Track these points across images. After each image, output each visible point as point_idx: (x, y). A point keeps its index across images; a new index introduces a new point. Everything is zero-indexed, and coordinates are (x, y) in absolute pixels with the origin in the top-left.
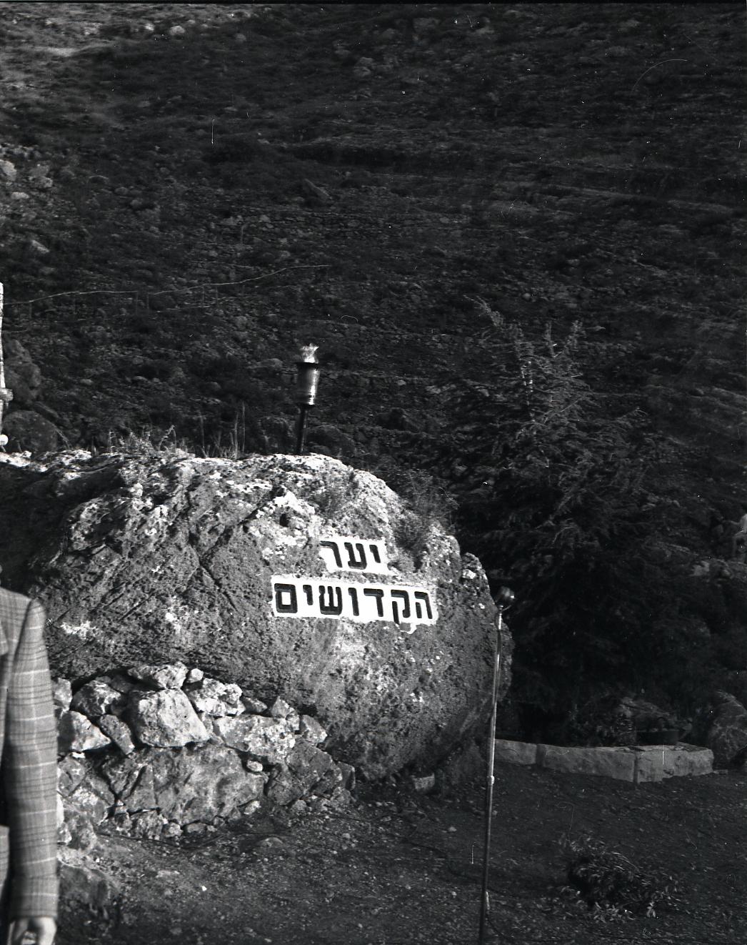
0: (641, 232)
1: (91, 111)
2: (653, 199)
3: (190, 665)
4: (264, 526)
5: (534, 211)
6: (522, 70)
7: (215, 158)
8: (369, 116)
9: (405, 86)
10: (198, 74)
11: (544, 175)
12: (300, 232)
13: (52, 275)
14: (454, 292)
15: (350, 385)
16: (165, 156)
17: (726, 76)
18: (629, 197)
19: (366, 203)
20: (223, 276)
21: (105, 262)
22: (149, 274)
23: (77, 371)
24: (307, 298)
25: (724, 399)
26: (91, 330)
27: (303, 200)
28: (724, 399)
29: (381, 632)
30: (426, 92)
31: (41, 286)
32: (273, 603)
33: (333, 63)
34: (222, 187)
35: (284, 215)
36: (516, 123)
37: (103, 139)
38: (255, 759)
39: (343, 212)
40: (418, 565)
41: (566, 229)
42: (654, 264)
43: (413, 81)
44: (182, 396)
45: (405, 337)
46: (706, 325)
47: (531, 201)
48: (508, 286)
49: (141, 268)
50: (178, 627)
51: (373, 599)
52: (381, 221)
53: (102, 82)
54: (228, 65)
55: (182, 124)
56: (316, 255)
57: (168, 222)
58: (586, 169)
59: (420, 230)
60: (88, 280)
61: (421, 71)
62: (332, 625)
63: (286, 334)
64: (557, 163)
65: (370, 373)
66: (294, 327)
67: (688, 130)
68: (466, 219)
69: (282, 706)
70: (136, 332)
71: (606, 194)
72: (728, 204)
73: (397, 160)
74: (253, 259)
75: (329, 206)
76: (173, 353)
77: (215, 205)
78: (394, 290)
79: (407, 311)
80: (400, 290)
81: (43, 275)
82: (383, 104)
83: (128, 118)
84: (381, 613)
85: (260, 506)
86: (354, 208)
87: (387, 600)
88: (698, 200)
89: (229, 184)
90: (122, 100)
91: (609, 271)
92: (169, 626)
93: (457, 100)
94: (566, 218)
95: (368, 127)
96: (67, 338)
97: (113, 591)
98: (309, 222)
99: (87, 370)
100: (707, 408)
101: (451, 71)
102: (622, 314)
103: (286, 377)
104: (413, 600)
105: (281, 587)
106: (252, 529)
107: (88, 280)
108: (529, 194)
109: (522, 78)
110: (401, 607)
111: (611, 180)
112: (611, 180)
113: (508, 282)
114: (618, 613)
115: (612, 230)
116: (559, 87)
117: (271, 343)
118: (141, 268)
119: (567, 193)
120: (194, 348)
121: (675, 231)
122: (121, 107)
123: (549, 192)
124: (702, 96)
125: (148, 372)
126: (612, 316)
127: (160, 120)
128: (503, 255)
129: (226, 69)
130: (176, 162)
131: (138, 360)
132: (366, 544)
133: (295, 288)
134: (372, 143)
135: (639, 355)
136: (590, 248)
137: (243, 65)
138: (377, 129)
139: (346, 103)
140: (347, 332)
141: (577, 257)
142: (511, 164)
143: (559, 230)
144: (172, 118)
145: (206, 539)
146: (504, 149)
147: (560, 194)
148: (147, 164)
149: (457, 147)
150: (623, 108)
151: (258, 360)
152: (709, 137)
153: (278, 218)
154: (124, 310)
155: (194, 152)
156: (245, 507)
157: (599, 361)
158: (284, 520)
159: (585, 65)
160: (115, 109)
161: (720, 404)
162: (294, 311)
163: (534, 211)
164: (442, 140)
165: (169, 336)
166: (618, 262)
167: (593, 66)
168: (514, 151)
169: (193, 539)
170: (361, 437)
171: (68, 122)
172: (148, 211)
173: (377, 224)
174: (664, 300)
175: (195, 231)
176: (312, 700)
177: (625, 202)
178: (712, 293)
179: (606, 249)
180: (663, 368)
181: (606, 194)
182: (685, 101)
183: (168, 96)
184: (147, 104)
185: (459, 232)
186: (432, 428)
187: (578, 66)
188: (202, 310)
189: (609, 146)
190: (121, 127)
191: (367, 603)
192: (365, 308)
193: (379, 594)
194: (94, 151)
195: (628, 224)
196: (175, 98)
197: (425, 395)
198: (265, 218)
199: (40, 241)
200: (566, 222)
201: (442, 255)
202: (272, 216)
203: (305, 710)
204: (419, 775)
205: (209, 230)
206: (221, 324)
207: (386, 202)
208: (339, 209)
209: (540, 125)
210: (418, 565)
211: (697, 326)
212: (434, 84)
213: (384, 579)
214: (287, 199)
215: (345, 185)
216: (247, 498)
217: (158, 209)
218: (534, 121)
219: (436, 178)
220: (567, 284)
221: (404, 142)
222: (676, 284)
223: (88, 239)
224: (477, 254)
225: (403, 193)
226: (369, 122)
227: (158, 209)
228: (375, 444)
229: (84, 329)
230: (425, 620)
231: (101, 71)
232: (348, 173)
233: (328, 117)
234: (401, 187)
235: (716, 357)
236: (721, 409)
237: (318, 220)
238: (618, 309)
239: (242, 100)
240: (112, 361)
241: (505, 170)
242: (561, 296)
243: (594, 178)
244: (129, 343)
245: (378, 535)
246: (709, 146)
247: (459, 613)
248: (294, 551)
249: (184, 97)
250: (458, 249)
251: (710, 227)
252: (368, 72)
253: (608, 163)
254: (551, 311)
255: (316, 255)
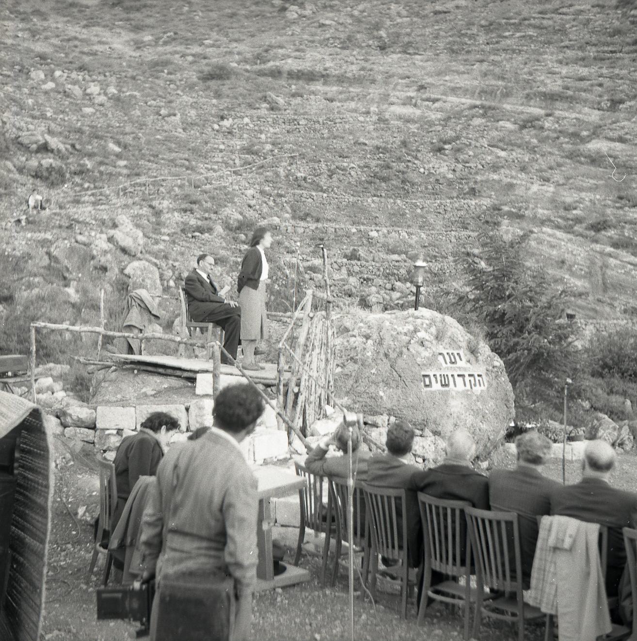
0: (487, 126)
1: (112, 43)
2: (493, 104)
3: (389, 415)
4: (414, 347)
5: (418, 112)
6: (399, 14)
7: (211, 77)
8: (301, 47)
9: (322, 25)
10: (182, 17)
11: (422, 88)
12: (271, 129)
13: (126, 166)
14: (377, 170)
15: (323, 233)
16: (172, 77)
17: (532, 21)
18: (478, 103)
19: (308, 107)
20: (231, 162)
21: (157, 156)
22: (187, 163)
23: (156, 231)
24: (287, 176)
25: (549, 235)
26: (160, 203)
27: (268, 106)
28: (549, 235)
29: (467, 395)
30: (337, 30)
31: (120, 174)
32: (422, 384)
33: (271, 10)
34: (215, 97)
35: (259, 118)
36: (400, 52)
37: (124, 64)
38: (419, 456)
39: (295, 114)
40: (477, 360)
41: (440, 124)
42: (498, 147)
43: (328, 22)
44: (224, 244)
45: (351, 200)
46: (535, 188)
47: (415, 105)
48: (410, 164)
49: (181, 159)
50: (385, 398)
51: (461, 379)
52: (321, 120)
53: (117, 23)
54: (202, 11)
55: (176, 52)
56: (287, 146)
57: (187, 126)
58: (449, 84)
59: (347, 126)
60: (149, 169)
61: (331, 15)
62: (447, 393)
63: (278, 200)
64: (429, 80)
65: (334, 225)
66: (281, 196)
67: (512, 58)
68: (375, 118)
69: (427, 432)
70: (189, 204)
71: (463, 100)
72: (541, 108)
73: (325, 77)
74: (249, 150)
75: (285, 110)
76: (213, 216)
77: (213, 112)
78: (340, 169)
79: (349, 183)
80: (344, 169)
81: (120, 167)
82: (311, 39)
83: (139, 48)
84: (465, 385)
85: (412, 338)
86: (302, 111)
87: (467, 379)
88: (522, 104)
89: (218, 95)
90: (132, 36)
91: (471, 153)
92: (381, 397)
93: (358, 36)
94: (439, 116)
95: (302, 54)
96: (145, 209)
97: (356, 382)
98: (275, 122)
99: (163, 230)
100: (540, 242)
101: (352, 16)
102: (482, 181)
103: (283, 228)
104: (477, 378)
105: (425, 376)
106: (411, 350)
107: (149, 169)
108: (414, 101)
109: (399, 20)
110: (473, 382)
111: (466, 92)
112: (466, 92)
113: (409, 161)
114: (25, 294)
115: (469, 125)
116: (424, 27)
117: (271, 208)
118: (181, 159)
119: (437, 100)
120: (226, 213)
121: (509, 126)
122: (133, 40)
123: (428, 100)
124: (518, 34)
125: (201, 230)
126: (476, 182)
127: (160, 49)
128: (404, 144)
129: (200, 14)
130: (181, 80)
131: (193, 222)
132: (455, 352)
133: (279, 169)
134: (304, 65)
135: (496, 208)
136: (458, 138)
137: (211, 11)
138: (308, 56)
139: (285, 38)
140: (315, 198)
141: (450, 143)
142: (400, 81)
143: (435, 125)
144: (169, 48)
145: (393, 355)
146: (394, 70)
147: (435, 101)
148: (161, 83)
149: (363, 69)
150: (469, 42)
151: (264, 218)
152: (526, 63)
153: (255, 119)
154: (176, 189)
155: (191, 73)
156: (406, 339)
157: (470, 212)
158: (422, 344)
159: (440, 12)
160: (127, 41)
161: (548, 239)
162: (280, 185)
163: (418, 112)
164: (352, 64)
165: (209, 205)
166: (476, 147)
167: (445, 12)
168: (400, 71)
169: (386, 355)
170: (335, 266)
171: (97, 51)
172: (173, 118)
173: (318, 122)
174: (507, 172)
175: (205, 131)
176: (440, 429)
177: (475, 107)
178: (536, 167)
179: (467, 138)
180: (512, 216)
181: (463, 100)
182: (506, 37)
183: (165, 33)
184: (150, 38)
185: (372, 127)
186: (376, 259)
187: (436, 13)
188: (225, 187)
189: (462, 68)
190: (134, 54)
191: (459, 381)
192: (323, 181)
193: (462, 376)
194: (124, 74)
195: (477, 121)
196: (169, 34)
197: (369, 238)
198: (246, 120)
199: (114, 143)
200: (440, 120)
201: (366, 144)
202: (251, 117)
203: (436, 433)
204: (482, 461)
205: (213, 130)
206: (238, 196)
207: (321, 107)
208: (292, 112)
209: (415, 54)
210: (477, 360)
211: (529, 189)
212: (342, 24)
213: (465, 369)
214: (257, 106)
215: (294, 95)
216: (406, 334)
217: (179, 116)
218: (411, 51)
219: (351, 89)
220: (445, 161)
221: (328, 65)
222: (514, 161)
223: (143, 140)
224: (387, 143)
225: (331, 100)
226: (303, 51)
227: (179, 116)
228: (344, 271)
229: (155, 203)
230: (482, 388)
231: (115, 15)
232: (293, 87)
233: (275, 47)
234: (329, 96)
235: (543, 208)
236: (549, 242)
237: (281, 121)
238: (479, 178)
239: (214, 35)
240: (177, 223)
241: (397, 84)
242: (442, 170)
243: (454, 90)
244: (185, 211)
245: (460, 347)
246: (526, 70)
247: (494, 383)
248: (428, 358)
249: (175, 33)
250: (373, 139)
251: (528, 123)
252: (296, 16)
253: (463, 81)
254: (437, 180)
255: (287, 146)
